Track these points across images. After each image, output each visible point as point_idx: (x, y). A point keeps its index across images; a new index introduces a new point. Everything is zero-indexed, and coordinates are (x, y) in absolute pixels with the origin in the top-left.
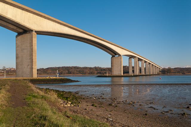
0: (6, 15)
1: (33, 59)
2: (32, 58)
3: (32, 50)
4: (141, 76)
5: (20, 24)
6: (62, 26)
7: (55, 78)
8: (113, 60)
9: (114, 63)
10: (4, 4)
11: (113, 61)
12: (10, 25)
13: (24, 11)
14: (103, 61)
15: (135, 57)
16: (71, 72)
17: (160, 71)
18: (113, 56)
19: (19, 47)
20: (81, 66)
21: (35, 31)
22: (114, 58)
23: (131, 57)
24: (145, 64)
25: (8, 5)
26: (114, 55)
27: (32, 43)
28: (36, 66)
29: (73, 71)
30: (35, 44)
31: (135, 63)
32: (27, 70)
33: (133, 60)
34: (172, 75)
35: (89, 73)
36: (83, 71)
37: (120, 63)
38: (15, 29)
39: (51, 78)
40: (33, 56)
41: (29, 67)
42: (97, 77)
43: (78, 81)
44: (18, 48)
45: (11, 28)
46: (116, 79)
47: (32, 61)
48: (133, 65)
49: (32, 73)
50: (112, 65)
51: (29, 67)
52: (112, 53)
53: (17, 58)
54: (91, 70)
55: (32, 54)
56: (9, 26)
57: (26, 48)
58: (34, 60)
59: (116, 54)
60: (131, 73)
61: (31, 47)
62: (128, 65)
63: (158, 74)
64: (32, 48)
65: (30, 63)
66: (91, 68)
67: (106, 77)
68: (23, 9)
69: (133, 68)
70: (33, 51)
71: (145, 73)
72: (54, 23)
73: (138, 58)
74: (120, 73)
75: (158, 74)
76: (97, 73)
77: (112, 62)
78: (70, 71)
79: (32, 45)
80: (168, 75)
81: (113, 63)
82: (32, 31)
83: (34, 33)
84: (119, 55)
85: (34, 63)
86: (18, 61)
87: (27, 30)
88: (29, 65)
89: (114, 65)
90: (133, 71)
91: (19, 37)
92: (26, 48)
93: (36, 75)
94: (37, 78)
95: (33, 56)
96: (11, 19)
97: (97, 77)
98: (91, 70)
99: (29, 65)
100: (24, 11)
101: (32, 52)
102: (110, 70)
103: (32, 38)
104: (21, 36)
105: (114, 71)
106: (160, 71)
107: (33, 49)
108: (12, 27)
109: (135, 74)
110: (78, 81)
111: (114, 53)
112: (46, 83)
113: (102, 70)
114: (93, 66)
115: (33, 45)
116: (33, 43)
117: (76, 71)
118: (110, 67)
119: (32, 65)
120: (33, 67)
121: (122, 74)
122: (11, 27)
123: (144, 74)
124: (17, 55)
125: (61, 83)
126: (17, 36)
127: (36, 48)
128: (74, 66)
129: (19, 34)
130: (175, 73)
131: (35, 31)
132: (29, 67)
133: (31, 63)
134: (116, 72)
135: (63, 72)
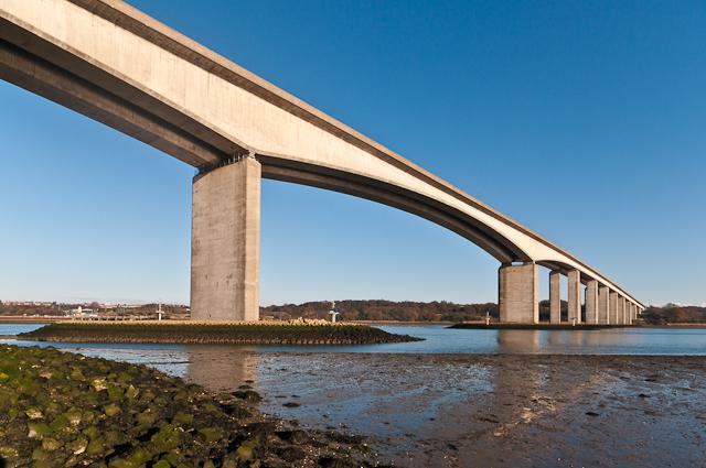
0: (143, 83)
1: (244, 255)
2: (244, 249)
3: (245, 222)
4: (608, 330)
5: (201, 122)
6: (351, 146)
7: (323, 322)
8: (505, 277)
9: (508, 285)
10: (137, 38)
11: (505, 280)
12: (169, 133)
13: (213, 78)
14: (468, 278)
15: (573, 269)
16: (367, 315)
17: (639, 316)
18: (505, 264)
19: (201, 215)
20: (397, 301)
21: (258, 157)
22: (508, 268)
23: (558, 268)
24: (581, 287)
25: (155, 46)
26: (509, 259)
27: (244, 196)
28: (254, 278)
29: (374, 312)
30: (256, 189)
31: (573, 289)
32: (223, 291)
33: (563, 279)
34: (681, 327)
35: (419, 319)
36: (403, 312)
37: (529, 285)
38: (187, 148)
39: (310, 322)
40: (248, 242)
41: (234, 281)
42: (420, 340)
43: (407, 339)
44: (198, 219)
45: (172, 144)
46: (514, 337)
47: (244, 262)
48: (564, 297)
49: (243, 302)
50: (502, 290)
51: (231, 284)
52: (503, 254)
53: (194, 253)
54: (426, 311)
55: (244, 234)
56: (166, 138)
57: (223, 214)
58: (248, 259)
59: (515, 258)
60: (556, 318)
61: (240, 212)
62: (497, 303)
63: (636, 325)
64: (245, 215)
65: (236, 270)
66: (422, 305)
67: (484, 327)
68: (212, 68)
69: (564, 305)
70: (248, 224)
71: (583, 319)
72: (326, 133)
73: (581, 272)
74: (529, 317)
75: (636, 325)
76: (441, 320)
77: (502, 282)
78: (366, 312)
79: (245, 205)
80: (669, 327)
81: (505, 284)
82: (245, 152)
83: (253, 168)
84: (527, 259)
85: (247, 267)
86: (198, 264)
87: (227, 150)
88: (231, 277)
89: (508, 290)
90: (564, 314)
91: (203, 181)
92: (223, 214)
93: (258, 315)
94: (260, 323)
95: (245, 244)
96: (162, 97)
97: (420, 340)
98: (426, 311)
99: (231, 277)
100: (215, 77)
101: (245, 228)
102: (494, 310)
103: (245, 177)
104: (209, 174)
105: (508, 309)
106: (639, 316)
107: (248, 218)
108: (176, 143)
109: (590, 321)
110: (407, 339)
111: (509, 254)
112: (290, 344)
113: (454, 311)
114: (427, 300)
115: (248, 203)
116: (248, 197)
117: (380, 313)
118: (548, 299)
119: (243, 276)
120: (246, 282)
121: (537, 321)
122: (171, 140)
123: (579, 322)
124: (194, 242)
125: (346, 344)
126: (195, 180)
127: (259, 212)
128: (376, 299)
129: (205, 169)
130: (693, 322)
131: (256, 155)
132: (231, 284)
133: (238, 267)
134: (513, 315)
135: (346, 314)
